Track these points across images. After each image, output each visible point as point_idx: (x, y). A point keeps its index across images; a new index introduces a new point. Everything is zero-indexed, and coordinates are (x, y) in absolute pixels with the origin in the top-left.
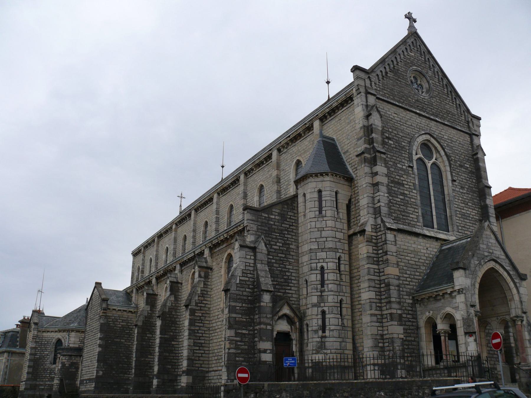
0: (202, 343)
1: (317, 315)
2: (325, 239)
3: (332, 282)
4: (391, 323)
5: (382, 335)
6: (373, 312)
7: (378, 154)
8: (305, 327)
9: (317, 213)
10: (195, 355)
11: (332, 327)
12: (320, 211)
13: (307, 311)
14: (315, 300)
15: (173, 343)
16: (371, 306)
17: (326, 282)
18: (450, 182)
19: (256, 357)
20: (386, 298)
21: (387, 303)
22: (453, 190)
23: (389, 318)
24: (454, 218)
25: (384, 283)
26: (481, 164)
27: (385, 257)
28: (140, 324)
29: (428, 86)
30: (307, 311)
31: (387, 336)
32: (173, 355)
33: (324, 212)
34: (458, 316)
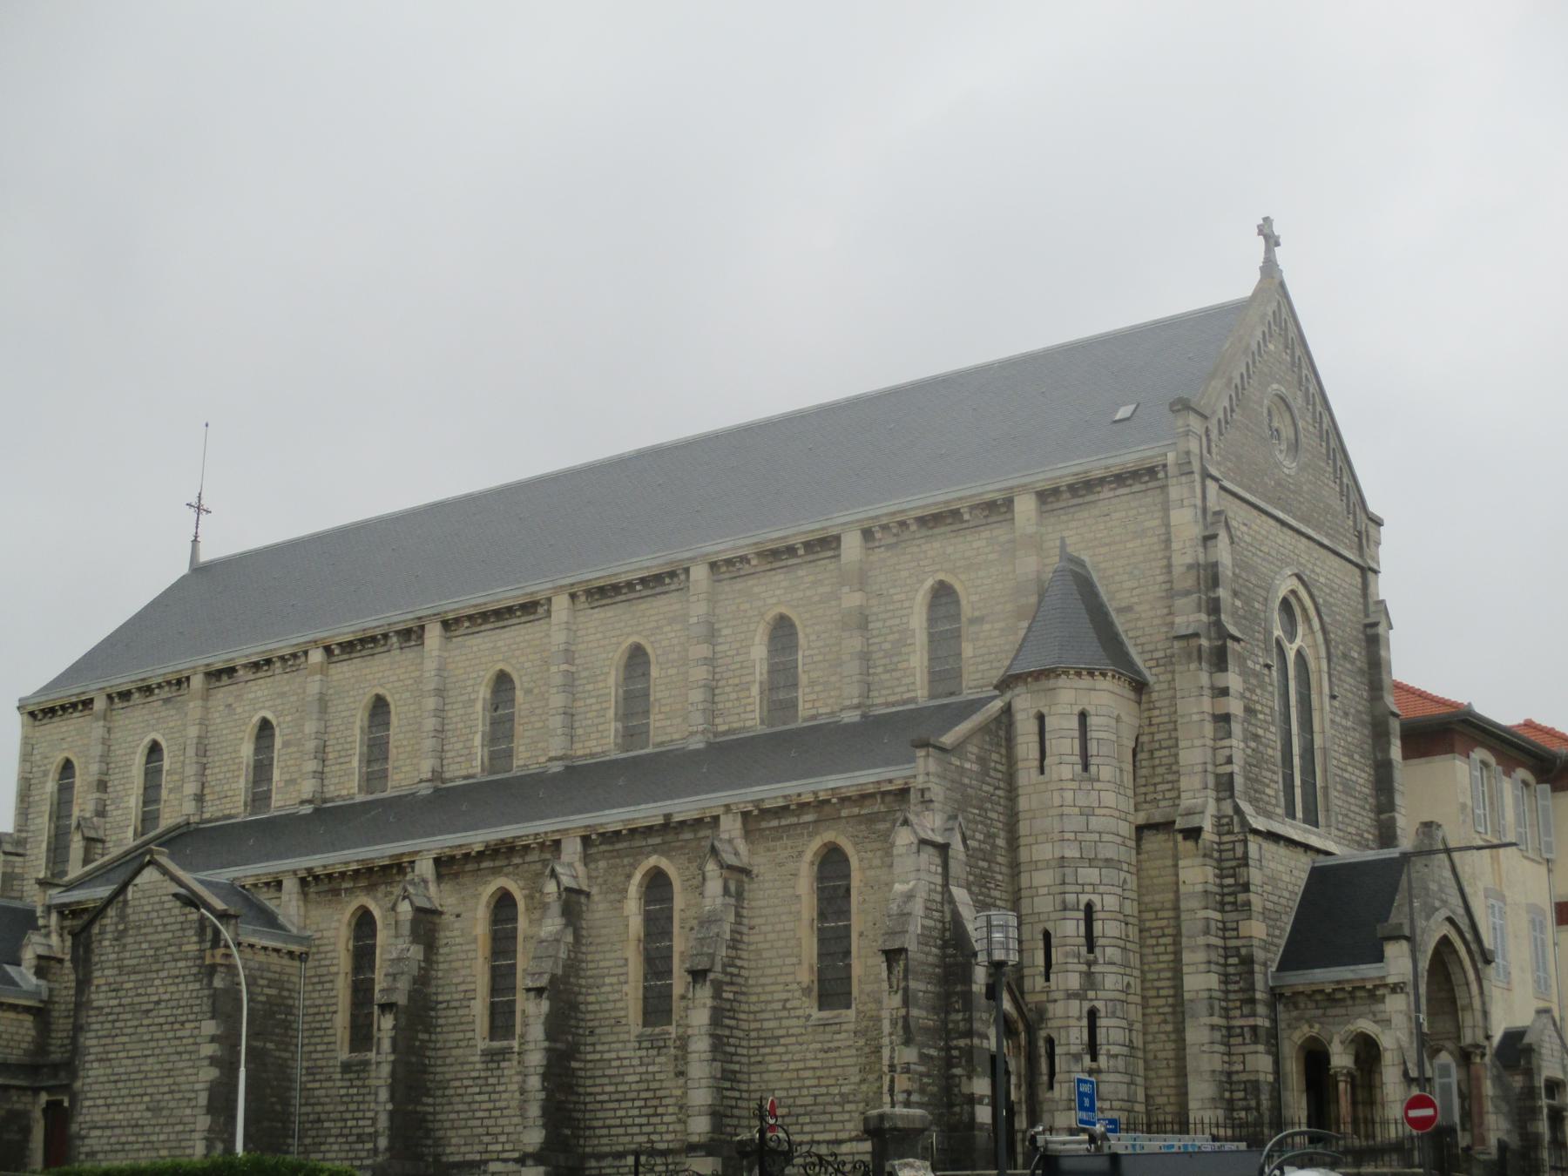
0: (734, 1072)
1: (1079, 1018)
2: (1096, 837)
3: (1114, 941)
4: (1252, 1048)
5: (1229, 1074)
6: (1216, 1020)
7: (1230, 643)
8: (1041, 1043)
9: (1078, 768)
10: (726, 1102)
11: (1115, 1050)
12: (1086, 768)
13: (1050, 1007)
14: (1074, 982)
15: (574, 1064)
16: (1212, 1007)
17: (1101, 942)
18: (1326, 699)
19: (955, 1114)
20: (1241, 990)
21: (1243, 1002)
22: (1332, 721)
23: (1247, 1036)
24: (1333, 793)
25: (1238, 955)
26: (1383, 653)
27: (1241, 897)
28: (401, 999)
29: (1292, 436)
30: (1050, 1007)
31: (1244, 1077)
32: (574, 1098)
33: (1093, 769)
34: (1386, 1041)
